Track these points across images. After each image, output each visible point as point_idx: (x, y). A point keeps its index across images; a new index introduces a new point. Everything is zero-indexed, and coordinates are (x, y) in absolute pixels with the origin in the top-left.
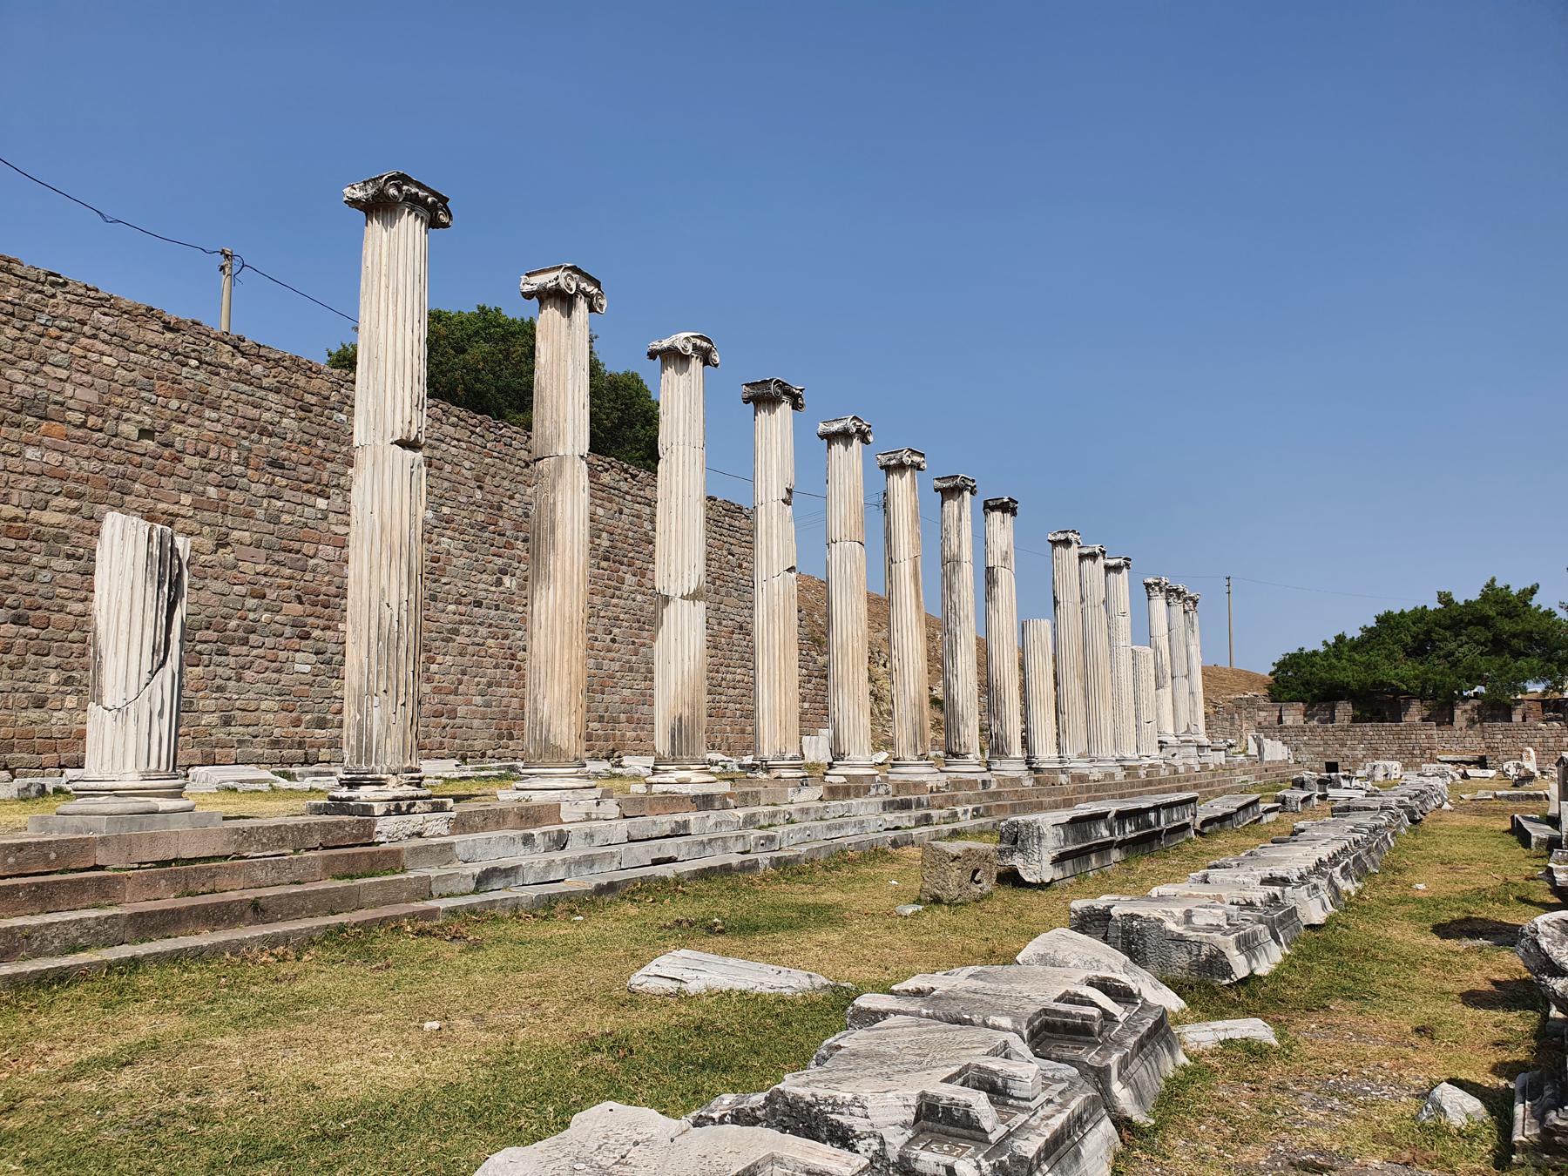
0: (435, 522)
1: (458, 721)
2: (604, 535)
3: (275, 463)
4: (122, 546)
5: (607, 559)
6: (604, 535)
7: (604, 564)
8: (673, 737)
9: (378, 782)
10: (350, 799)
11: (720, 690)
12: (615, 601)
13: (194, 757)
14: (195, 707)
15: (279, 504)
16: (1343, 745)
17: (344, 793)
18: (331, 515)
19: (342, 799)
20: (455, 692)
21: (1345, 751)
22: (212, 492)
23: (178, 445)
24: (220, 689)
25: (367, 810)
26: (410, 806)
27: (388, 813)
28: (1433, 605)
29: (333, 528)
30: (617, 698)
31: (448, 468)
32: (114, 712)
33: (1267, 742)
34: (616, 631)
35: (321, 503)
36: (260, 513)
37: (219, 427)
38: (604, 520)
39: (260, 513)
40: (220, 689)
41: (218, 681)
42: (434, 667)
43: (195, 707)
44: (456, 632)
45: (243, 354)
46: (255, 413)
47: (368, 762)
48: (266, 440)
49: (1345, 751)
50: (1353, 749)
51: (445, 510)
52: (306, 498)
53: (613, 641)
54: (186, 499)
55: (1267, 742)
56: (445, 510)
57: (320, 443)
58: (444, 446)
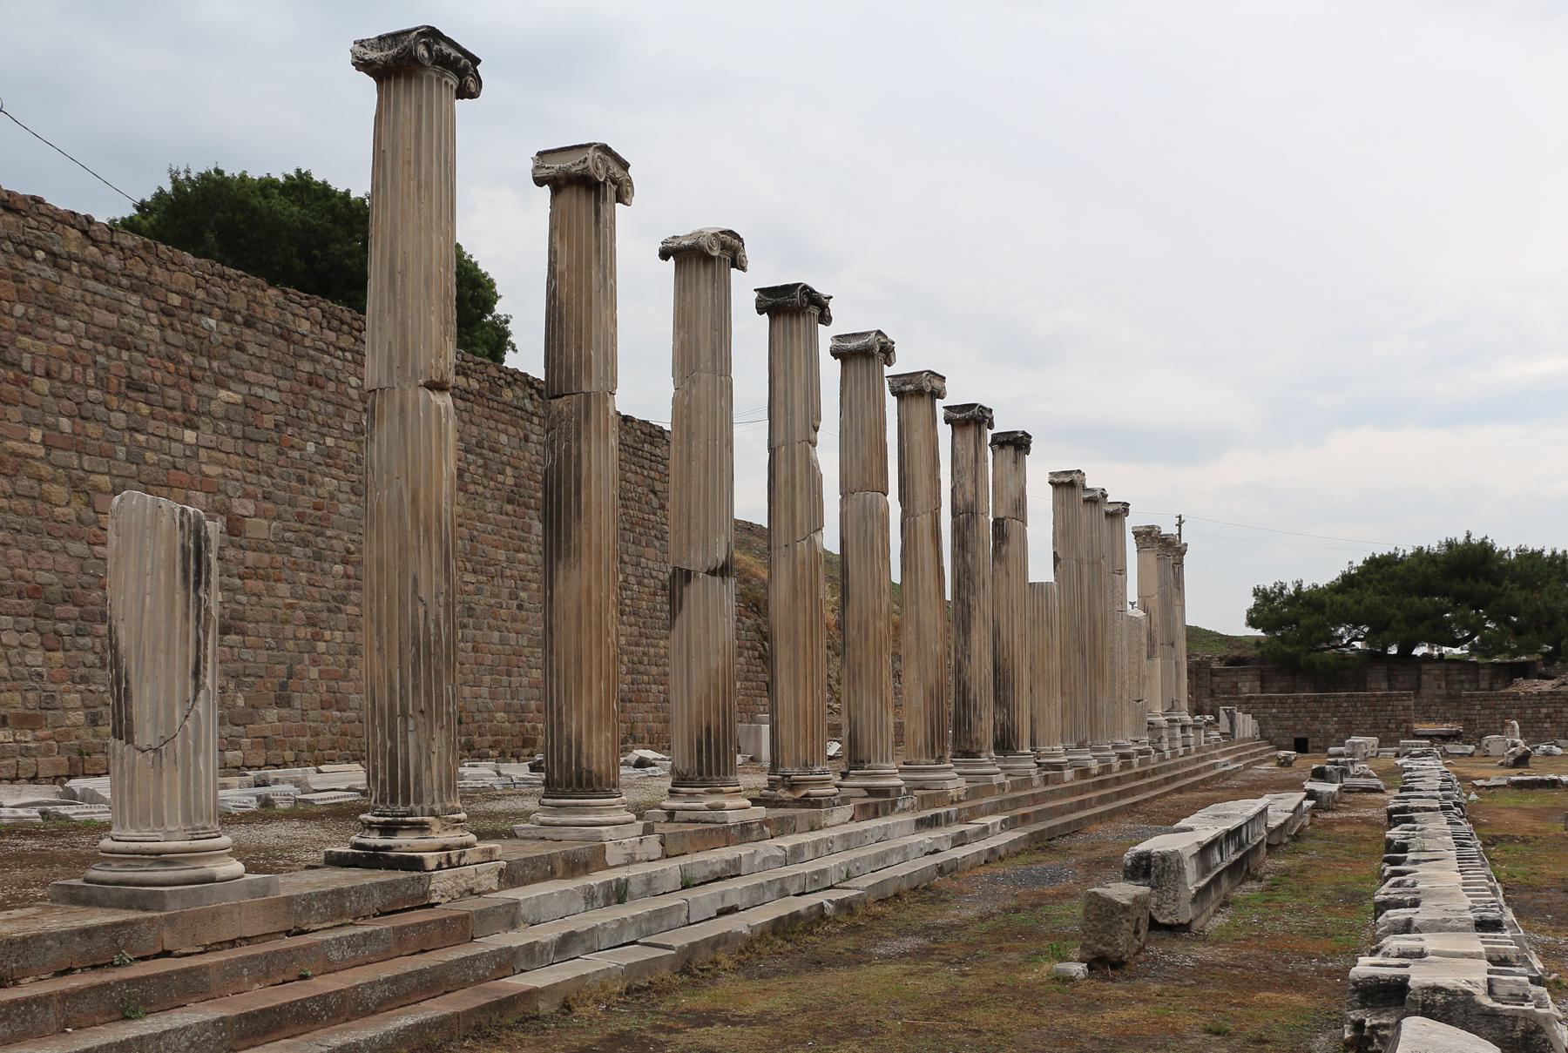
0: (317, 458)
1: (351, 714)
2: (509, 470)
3: (134, 385)
4: (142, 532)
5: (510, 501)
6: (509, 470)
7: (509, 508)
8: (700, 751)
9: (421, 827)
10: (389, 848)
11: (641, 668)
12: (521, 556)
13: (57, 766)
14: (58, 703)
15: (141, 438)
16: (1314, 718)
17: (375, 840)
18: (202, 452)
19: (376, 848)
20: (345, 678)
21: (1317, 725)
22: (65, 423)
23: (27, 365)
24: (84, 679)
25: (415, 864)
26: (460, 856)
27: (439, 867)
28: (1461, 540)
29: (204, 468)
30: (525, 680)
31: (331, 386)
32: (151, 755)
33: (1239, 716)
34: (523, 595)
35: (189, 436)
36: (121, 452)
37: (70, 339)
38: (508, 451)
39: (121, 452)
40: (84, 679)
41: (82, 671)
42: (321, 646)
43: (58, 703)
44: (343, 599)
45: (95, 242)
46: (112, 319)
47: (406, 801)
48: (125, 355)
49: (1317, 725)
50: (1325, 722)
51: (330, 441)
52: (173, 431)
53: (520, 607)
54: (36, 434)
55: (1239, 716)
56: (330, 441)
57: (187, 357)
58: (327, 358)
